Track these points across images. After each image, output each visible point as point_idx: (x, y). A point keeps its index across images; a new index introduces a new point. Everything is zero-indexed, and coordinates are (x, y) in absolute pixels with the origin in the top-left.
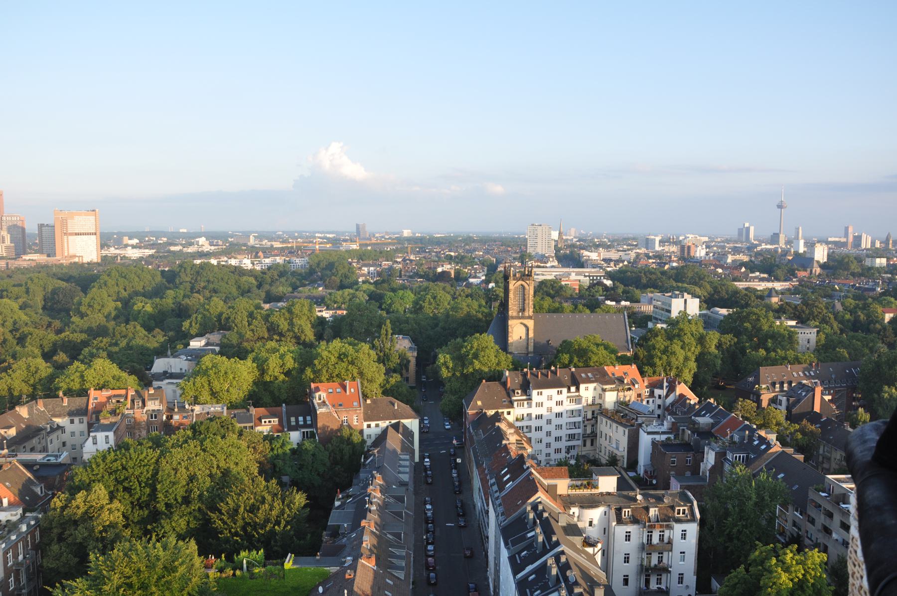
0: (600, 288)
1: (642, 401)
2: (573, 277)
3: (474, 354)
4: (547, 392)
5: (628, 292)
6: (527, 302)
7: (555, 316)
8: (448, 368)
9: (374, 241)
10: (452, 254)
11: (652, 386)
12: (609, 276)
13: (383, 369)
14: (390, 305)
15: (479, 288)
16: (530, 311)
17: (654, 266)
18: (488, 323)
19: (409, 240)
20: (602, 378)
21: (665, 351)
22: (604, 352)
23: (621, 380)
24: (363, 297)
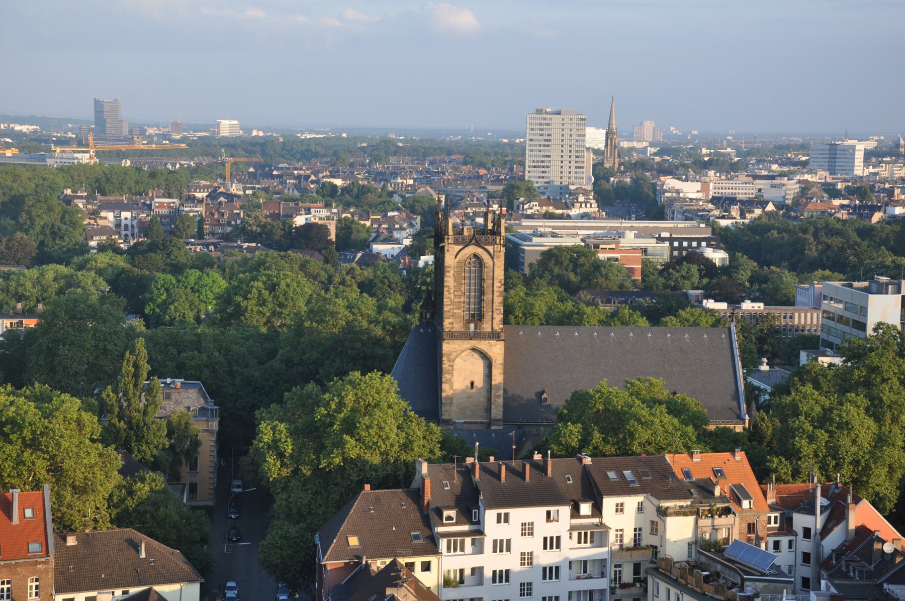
0: (694, 269)
1: (759, 539)
2: (630, 240)
3: (345, 420)
4: (519, 515)
5: (765, 280)
6: (487, 297)
7: (558, 332)
8: (281, 455)
9: (140, 145)
10: (338, 182)
11: (789, 507)
12: (722, 238)
13: (118, 460)
14: (165, 306)
15: (394, 268)
16: (495, 320)
17: (843, 215)
18: (397, 348)
19: (231, 145)
20: (659, 483)
21: (824, 420)
22: (667, 418)
23: (705, 489)
24: (93, 286)
